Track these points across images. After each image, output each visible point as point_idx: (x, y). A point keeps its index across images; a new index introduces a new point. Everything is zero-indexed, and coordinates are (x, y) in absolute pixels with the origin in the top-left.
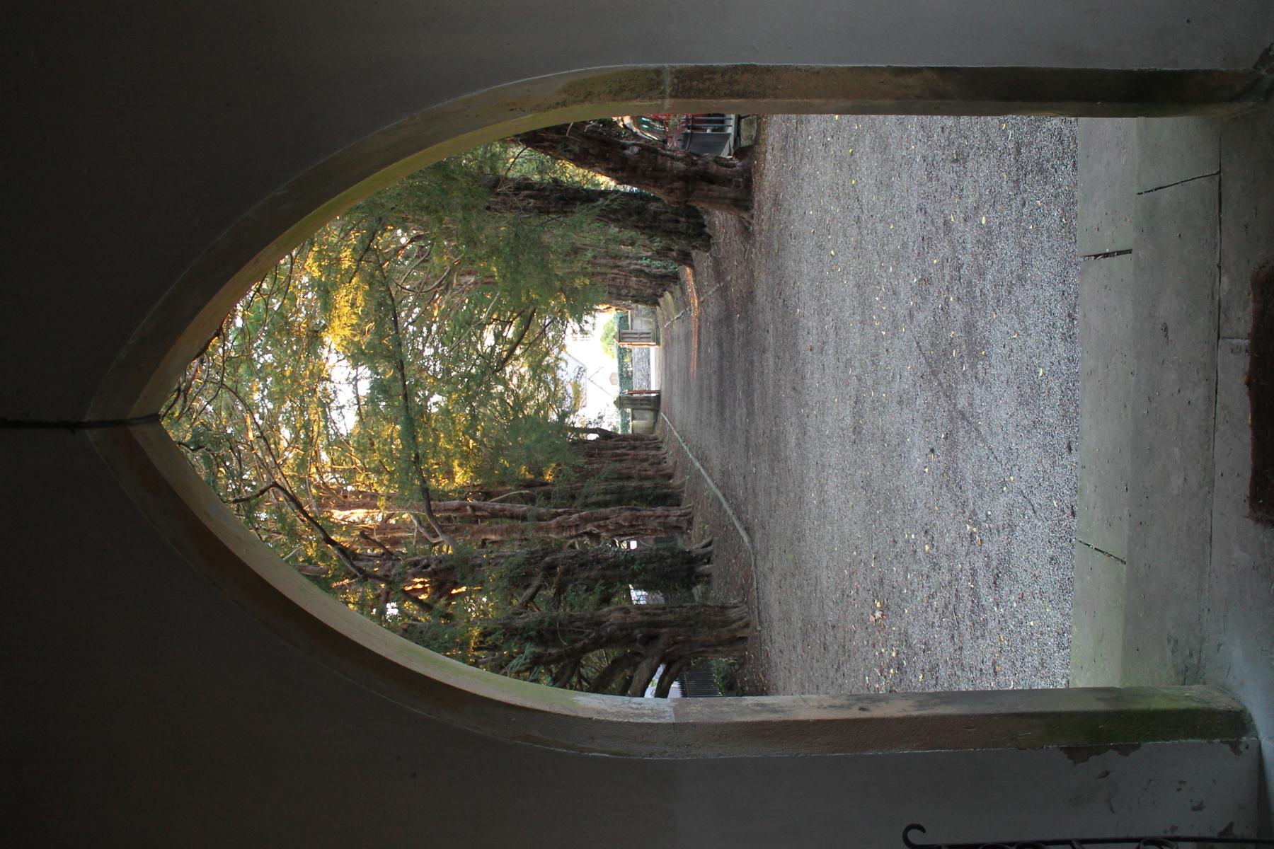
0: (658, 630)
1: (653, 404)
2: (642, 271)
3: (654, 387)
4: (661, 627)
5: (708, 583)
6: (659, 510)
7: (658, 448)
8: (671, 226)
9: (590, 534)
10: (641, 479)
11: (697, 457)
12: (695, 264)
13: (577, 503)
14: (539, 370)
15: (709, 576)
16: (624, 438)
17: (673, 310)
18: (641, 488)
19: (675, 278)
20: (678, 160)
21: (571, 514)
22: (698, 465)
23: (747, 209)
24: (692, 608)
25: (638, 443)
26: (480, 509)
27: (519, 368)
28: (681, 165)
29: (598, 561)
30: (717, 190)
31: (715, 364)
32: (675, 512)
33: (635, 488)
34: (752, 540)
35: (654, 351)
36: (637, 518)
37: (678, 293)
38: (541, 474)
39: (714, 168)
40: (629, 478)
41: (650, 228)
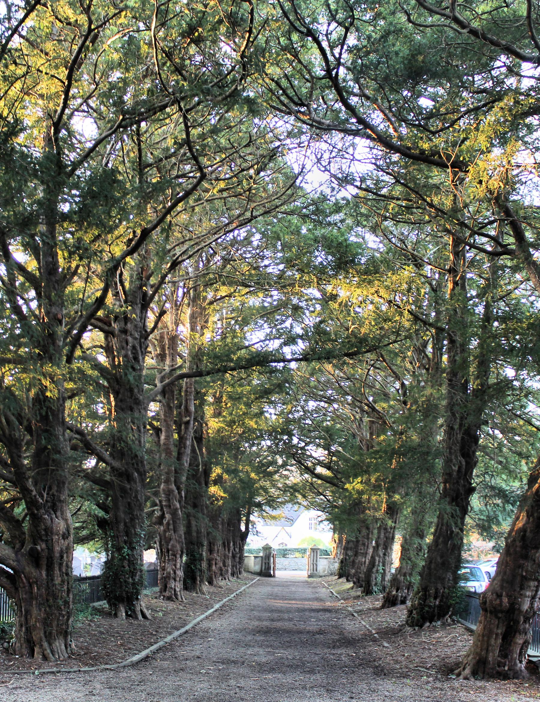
0: (44, 567)
1: (266, 572)
2: (374, 566)
3: (277, 573)
4: (48, 570)
5: (109, 614)
6: (180, 573)
7: (233, 575)
8: (432, 591)
9: (163, 516)
10: (209, 561)
11: (223, 606)
12: (385, 610)
13: (190, 510)
14: (293, 490)
15: (116, 615)
16: (241, 550)
17: (338, 588)
18: (201, 559)
19: (368, 591)
20: (532, 604)
21: (180, 502)
22: (217, 606)
23: (474, 673)
24: (66, 603)
25: (237, 560)
26: (187, 428)
27: (295, 476)
28: (526, 606)
29: (132, 520)
30: (496, 643)
31: (302, 626)
32: (179, 586)
33: (202, 555)
34: (135, 665)
35: (303, 575)
36: (175, 555)
37: (353, 593)
38: (215, 484)
39: (520, 640)
40: (211, 551)
41: (430, 574)
